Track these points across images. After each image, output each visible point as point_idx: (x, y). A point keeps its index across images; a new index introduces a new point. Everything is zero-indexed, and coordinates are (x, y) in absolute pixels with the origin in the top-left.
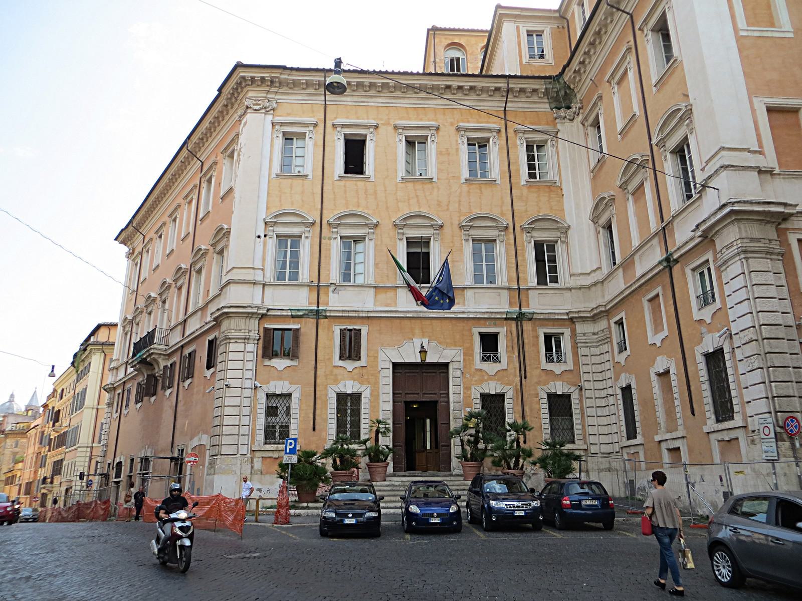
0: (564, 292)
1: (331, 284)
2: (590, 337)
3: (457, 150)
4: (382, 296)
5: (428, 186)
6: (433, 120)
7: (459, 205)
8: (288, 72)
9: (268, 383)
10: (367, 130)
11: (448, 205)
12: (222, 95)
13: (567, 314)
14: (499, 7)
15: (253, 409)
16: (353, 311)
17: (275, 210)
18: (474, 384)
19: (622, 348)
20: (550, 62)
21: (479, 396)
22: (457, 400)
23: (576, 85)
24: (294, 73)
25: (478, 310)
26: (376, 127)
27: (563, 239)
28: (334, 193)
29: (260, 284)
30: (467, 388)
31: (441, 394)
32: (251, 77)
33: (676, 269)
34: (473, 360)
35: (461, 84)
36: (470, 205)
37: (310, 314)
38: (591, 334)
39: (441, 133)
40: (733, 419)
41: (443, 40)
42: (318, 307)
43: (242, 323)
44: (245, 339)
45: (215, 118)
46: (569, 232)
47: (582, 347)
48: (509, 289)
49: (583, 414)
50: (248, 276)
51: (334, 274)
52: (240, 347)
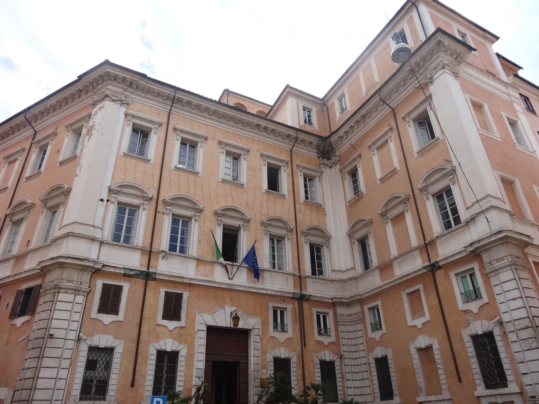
0: (329, 282)
1: (162, 251)
2: (346, 318)
3: (261, 169)
4: (202, 268)
5: (240, 189)
6: (245, 145)
7: (261, 207)
8: (147, 80)
9: (92, 335)
10: (199, 139)
11: (253, 206)
12: (81, 82)
13: (332, 299)
14: (288, 86)
15: (73, 362)
16: (179, 277)
17: (120, 181)
18: (268, 349)
19: (377, 326)
20: (317, 129)
21: (272, 360)
22: (257, 362)
23: (337, 146)
24: (151, 82)
25: (274, 289)
26: (206, 139)
27: (327, 245)
28: (170, 179)
29: (98, 241)
30: (264, 352)
31: (242, 356)
32: (115, 74)
33: (439, 274)
34: (268, 329)
35: (267, 125)
36: (268, 209)
37: (140, 274)
38: (347, 316)
39: (250, 155)
40: (507, 386)
41: (234, 100)
42: (148, 269)
43: (75, 275)
44: (76, 290)
45: (65, 98)
46: (331, 240)
47: (341, 325)
48: (294, 275)
49: (343, 378)
50: (90, 232)
51: (164, 243)
52: (70, 297)
